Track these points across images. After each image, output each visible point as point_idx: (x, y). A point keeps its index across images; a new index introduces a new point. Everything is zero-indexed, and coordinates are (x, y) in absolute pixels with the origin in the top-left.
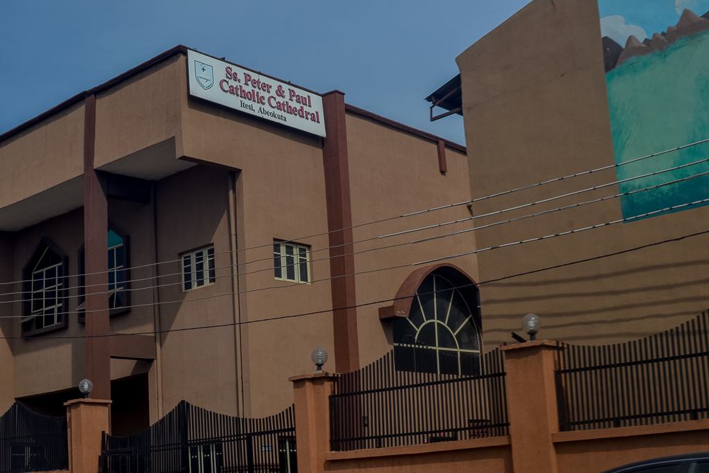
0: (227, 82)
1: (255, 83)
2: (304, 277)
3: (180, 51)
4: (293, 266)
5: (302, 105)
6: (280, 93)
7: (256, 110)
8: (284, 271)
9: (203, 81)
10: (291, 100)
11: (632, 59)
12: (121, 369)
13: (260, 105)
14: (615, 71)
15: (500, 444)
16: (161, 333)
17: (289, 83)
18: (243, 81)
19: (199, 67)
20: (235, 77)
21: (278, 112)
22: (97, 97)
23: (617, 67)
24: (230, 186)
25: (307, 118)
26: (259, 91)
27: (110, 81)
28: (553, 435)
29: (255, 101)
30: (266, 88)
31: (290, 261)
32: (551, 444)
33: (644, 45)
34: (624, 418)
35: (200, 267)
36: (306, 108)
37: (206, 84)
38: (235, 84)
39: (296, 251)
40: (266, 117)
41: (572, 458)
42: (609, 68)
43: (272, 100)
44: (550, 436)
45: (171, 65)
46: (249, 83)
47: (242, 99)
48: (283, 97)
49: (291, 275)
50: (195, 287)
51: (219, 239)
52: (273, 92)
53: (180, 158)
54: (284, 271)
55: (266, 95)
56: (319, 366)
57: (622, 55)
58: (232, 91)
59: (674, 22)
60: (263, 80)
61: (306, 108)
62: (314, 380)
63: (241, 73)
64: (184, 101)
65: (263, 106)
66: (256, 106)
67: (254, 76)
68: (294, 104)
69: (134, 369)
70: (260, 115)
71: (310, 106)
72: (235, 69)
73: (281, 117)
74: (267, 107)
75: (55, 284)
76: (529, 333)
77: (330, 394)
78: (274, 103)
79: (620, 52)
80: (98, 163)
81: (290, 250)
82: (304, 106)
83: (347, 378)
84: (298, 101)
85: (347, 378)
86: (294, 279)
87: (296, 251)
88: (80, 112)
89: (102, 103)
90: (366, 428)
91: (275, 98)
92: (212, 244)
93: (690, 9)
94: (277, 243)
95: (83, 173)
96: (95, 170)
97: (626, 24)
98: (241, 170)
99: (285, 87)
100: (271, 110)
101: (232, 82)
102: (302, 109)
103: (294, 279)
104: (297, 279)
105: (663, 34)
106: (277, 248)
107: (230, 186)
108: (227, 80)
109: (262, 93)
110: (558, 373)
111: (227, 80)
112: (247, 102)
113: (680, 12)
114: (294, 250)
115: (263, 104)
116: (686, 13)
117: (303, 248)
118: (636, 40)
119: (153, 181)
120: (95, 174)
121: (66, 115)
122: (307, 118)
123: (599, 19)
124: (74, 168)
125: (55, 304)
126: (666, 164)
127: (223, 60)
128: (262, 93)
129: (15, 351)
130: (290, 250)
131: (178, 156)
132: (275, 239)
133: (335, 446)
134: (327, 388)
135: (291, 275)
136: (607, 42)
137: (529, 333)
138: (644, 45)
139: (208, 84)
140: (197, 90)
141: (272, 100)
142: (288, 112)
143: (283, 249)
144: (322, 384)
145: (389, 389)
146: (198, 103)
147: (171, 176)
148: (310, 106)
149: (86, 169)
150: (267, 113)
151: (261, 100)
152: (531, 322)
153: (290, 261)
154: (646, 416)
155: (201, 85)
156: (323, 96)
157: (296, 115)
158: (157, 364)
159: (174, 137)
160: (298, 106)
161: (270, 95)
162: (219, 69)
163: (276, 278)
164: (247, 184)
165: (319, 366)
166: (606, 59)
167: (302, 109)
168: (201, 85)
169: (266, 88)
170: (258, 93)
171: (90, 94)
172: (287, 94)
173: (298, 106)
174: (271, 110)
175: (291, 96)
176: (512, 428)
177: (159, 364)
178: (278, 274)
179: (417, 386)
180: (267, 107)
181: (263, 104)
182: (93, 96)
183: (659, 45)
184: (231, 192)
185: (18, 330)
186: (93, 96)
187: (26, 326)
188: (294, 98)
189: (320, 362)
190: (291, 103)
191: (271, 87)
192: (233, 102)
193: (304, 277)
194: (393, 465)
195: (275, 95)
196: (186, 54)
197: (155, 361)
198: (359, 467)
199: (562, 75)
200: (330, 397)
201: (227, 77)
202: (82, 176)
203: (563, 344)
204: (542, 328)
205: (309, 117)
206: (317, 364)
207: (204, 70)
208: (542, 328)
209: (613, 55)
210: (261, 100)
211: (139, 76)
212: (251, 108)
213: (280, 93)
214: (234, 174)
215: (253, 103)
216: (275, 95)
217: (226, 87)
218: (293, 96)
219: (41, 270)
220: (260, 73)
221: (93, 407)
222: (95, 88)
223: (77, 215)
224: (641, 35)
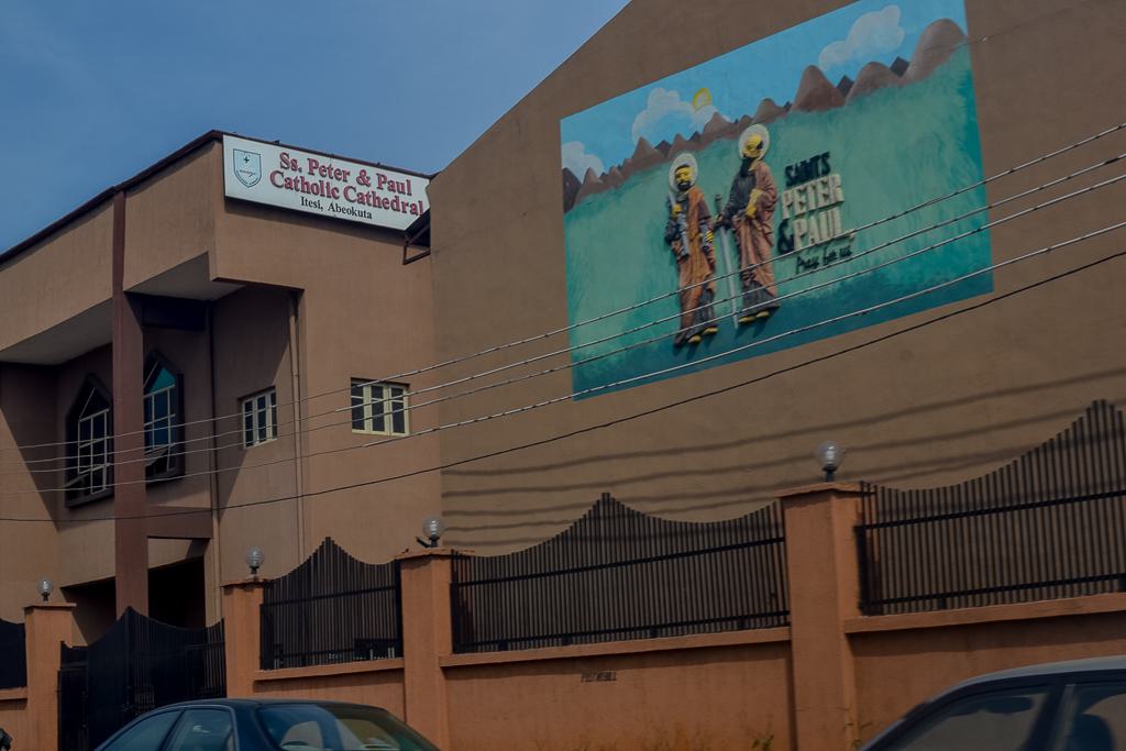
0: (282, 174)
1: (323, 170)
2: (399, 427)
3: (213, 138)
4: (382, 418)
5: (397, 194)
6: (363, 179)
7: (325, 207)
8: (388, 421)
9: (245, 176)
10: (380, 188)
11: (589, 198)
12: (165, 553)
13: (331, 200)
14: (571, 212)
15: (670, 648)
16: (218, 508)
17: (378, 166)
18: (306, 169)
19: (240, 157)
20: (294, 166)
21: (358, 207)
22: (128, 193)
23: (575, 207)
24: (292, 310)
25: (404, 212)
26: (330, 180)
27: (141, 174)
28: (440, 658)
29: (323, 195)
30: (342, 175)
31: (378, 408)
32: (843, 637)
33: (600, 181)
34: (952, 594)
35: (262, 417)
36: (403, 198)
37: (250, 180)
38: (292, 175)
39: (387, 393)
40: (340, 215)
41: (459, 685)
42: (568, 207)
43: (350, 192)
44: (437, 660)
45: (206, 156)
46: (316, 171)
47: (303, 195)
48: (368, 185)
49: (378, 425)
50: (257, 444)
51: (280, 381)
52: (352, 180)
53: (215, 280)
54: (388, 421)
55: (341, 186)
56: (254, 569)
57: (580, 192)
58: (289, 185)
59: (629, 153)
60: (337, 164)
61: (403, 198)
62: (243, 586)
63: (302, 159)
64: (221, 204)
65: (335, 202)
66: (326, 202)
67: (323, 161)
68: (385, 194)
69: (190, 550)
70: (331, 214)
71: (410, 194)
72: (293, 154)
73: (362, 214)
74: (342, 202)
75: (94, 445)
76: (825, 469)
77: (261, 602)
78: (352, 195)
79: (577, 190)
80: (129, 284)
81: (377, 392)
82: (401, 196)
83: (977, 486)
84: (391, 189)
85: (977, 486)
86: (383, 430)
87: (387, 393)
88: (107, 215)
89: (133, 202)
90: (773, 591)
91: (354, 189)
92: (274, 387)
93: (646, 137)
94: (356, 386)
95: (111, 296)
96: (126, 293)
97: (586, 153)
98: (303, 290)
99: (372, 172)
100: (348, 205)
101: (290, 174)
102: (396, 200)
103: (383, 430)
104: (389, 430)
105: (619, 167)
106: (357, 391)
107: (292, 310)
108: (282, 170)
109: (334, 183)
110: (860, 531)
111: (282, 170)
112: (311, 198)
113: (635, 142)
114: (384, 391)
115: (337, 198)
116: (642, 142)
117: (399, 388)
118: (594, 173)
119: (208, 302)
120: (125, 299)
121: (94, 217)
122: (404, 212)
123: (559, 144)
124: (100, 291)
125: (103, 462)
126: (614, 329)
127: (277, 143)
128: (334, 183)
129: (59, 523)
130: (377, 392)
131: (212, 278)
132: (353, 379)
133: (266, 664)
134: (258, 594)
135: (378, 425)
136: (567, 175)
137: (825, 469)
138: (600, 181)
139: (253, 178)
140: (234, 189)
141: (350, 192)
142: (375, 206)
143: (367, 392)
144: (252, 591)
145: (688, 554)
146: (236, 205)
147: (225, 297)
148: (410, 194)
149: (115, 293)
150: (342, 210)
151: (333, 194)
152: (830, 453)
153: (378, 408)
154: (902, 600)
155: (245, 183)
156: (431, 178)
157: (386, 208)
158: (214, 545)
159: (207, 253)
160: (391, 196)
161: (346, 185)
162: (270, 156)
163: (354, 431)
164: (309, 305)
165: (254, 569)
166: (565, 195)
167: (396, 200)
168: (245, 183)
169: (342, 175)
170: (328, 184)
171: (118, 192)
172: (374, 182)
173: (391, 196)
174: (348, 205)
175: (380, 183)
176: (793, 618)
177: (216, 545)
178: (360, 425)
179: (709, 551)
180: (342, 202)
181: (337, 198)
182: (122, 193)
183: (615, 180)
184: (292, 319)
185: (62, 500)
186: (122, 193)
187: (70, 495)
188: (385, 186)
189: (254, 564)
190: (379, 193)
191: (348, 173)
192: (291, 200)
193: (399, 427)
194: (310, 688)
195: (355, 185)
196: (221, 141)
197: (211, 541)
198: (283, 690)
199: (525, 214)
200: (261, 605)
201: (282, 167)
202: (562, 118)
203: (876, 487)
204: (447, 529)
205: (408, 209)
206: (251, 567)
207: (247, 160)
208: (447, 529)
209: (572, 191)
210: (333, 194)
211: (171, 168)
212: (317, 205)
213: (363, 179)
214: (295, 295)
215: (318, 198)
216: (355, 185)
217: (279, 180)
218: (384, 182)
219: (88, 418)
220: (333, 157)
221: (52, 612)
222: (123, 184)
223: (103, 353)
224: (599, 170)
